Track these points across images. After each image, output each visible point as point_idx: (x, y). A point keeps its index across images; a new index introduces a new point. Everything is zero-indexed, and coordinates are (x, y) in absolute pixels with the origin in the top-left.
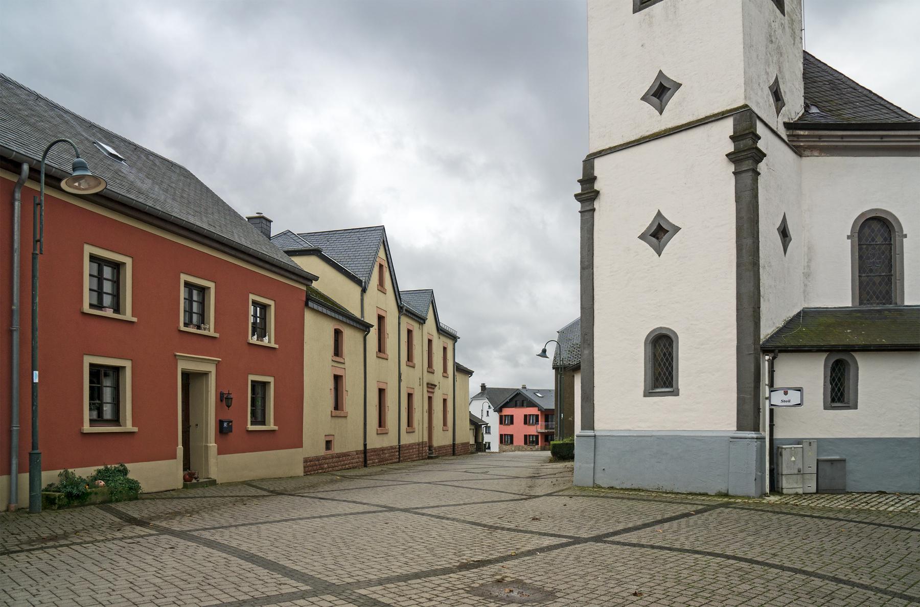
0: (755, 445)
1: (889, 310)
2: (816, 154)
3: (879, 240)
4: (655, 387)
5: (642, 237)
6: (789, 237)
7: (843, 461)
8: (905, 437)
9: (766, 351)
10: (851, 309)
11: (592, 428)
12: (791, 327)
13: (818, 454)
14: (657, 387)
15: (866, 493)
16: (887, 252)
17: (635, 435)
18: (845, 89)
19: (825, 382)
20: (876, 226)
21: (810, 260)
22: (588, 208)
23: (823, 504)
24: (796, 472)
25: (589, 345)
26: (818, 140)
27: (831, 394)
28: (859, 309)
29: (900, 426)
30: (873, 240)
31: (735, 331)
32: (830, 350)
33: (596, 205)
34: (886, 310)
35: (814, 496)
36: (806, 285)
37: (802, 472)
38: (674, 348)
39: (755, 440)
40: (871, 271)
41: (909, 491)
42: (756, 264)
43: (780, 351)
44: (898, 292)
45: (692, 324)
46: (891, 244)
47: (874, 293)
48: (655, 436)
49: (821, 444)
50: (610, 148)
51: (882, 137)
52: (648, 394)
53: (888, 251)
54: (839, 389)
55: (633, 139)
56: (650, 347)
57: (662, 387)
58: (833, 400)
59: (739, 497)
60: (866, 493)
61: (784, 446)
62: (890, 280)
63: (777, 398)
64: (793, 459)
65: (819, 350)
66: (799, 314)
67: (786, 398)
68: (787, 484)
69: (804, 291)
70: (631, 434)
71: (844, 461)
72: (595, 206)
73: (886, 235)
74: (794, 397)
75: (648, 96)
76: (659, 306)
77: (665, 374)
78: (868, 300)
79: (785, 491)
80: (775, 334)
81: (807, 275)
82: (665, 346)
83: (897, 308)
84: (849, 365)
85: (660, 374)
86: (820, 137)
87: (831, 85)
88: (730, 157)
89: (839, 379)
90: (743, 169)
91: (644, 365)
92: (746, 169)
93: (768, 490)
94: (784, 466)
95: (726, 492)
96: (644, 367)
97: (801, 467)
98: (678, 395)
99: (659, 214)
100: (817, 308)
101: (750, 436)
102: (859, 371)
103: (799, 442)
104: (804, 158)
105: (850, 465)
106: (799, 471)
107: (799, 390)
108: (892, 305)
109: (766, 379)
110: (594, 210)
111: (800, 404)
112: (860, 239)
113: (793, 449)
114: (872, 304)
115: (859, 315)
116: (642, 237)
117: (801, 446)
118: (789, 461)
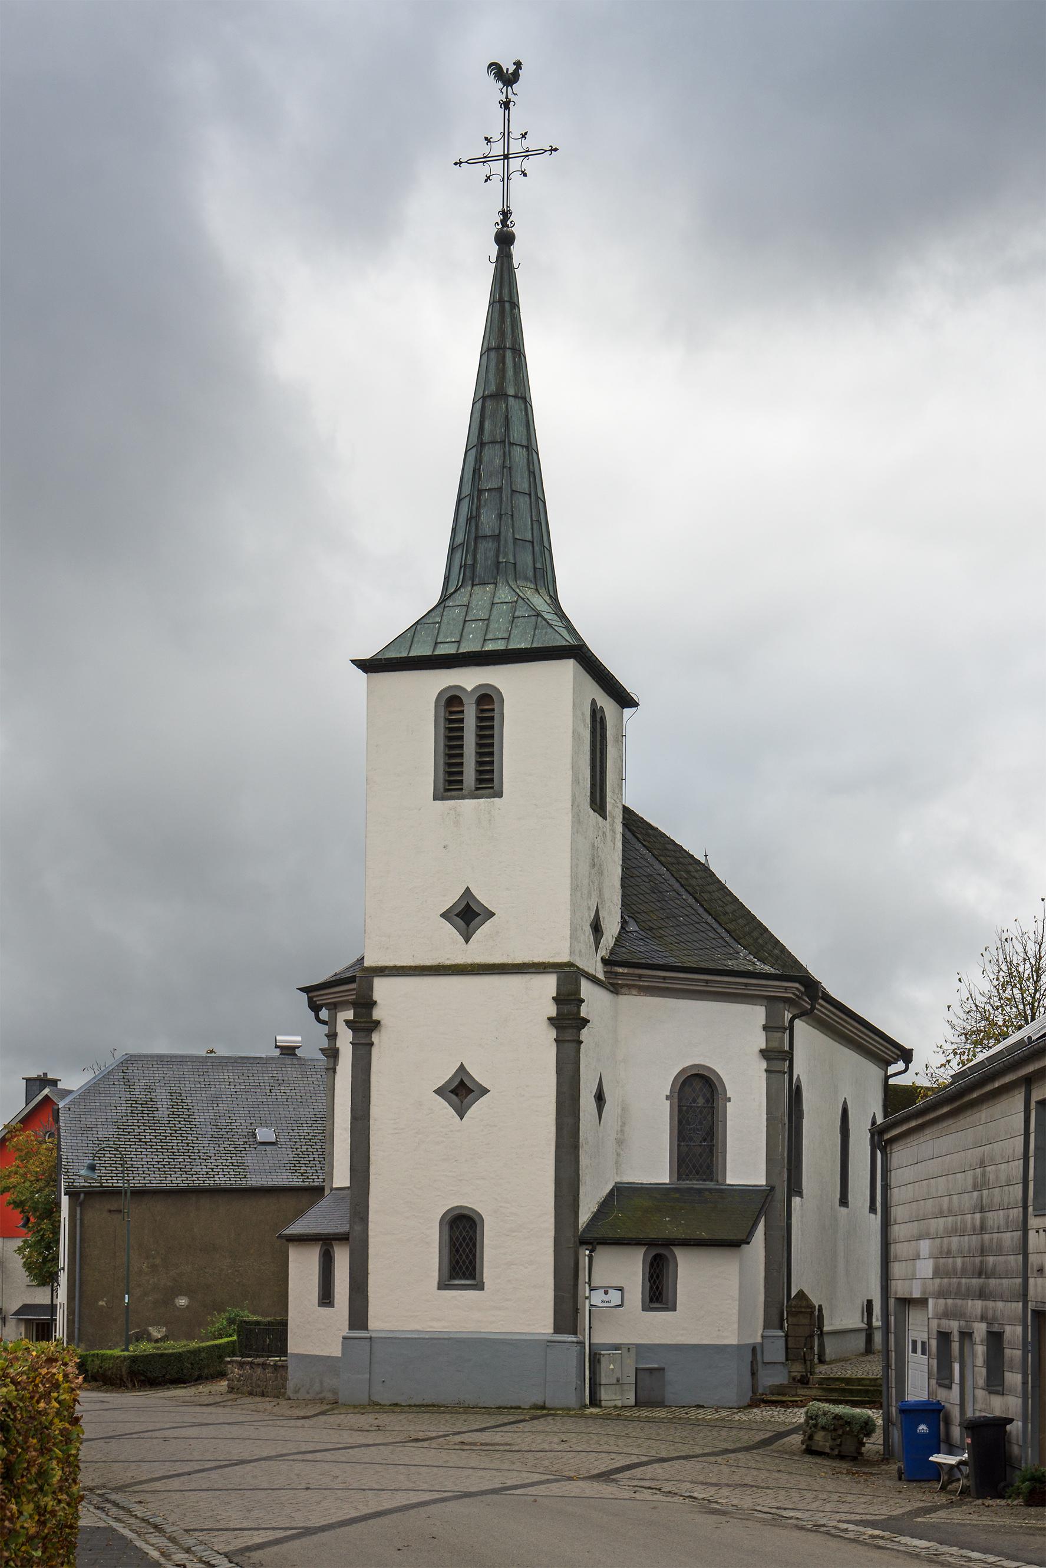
0: (576, 1349)
1: (710, 1190)
2: (634, 992)
3: (701, 1101)
4: (452, 1277)
5: (439, 1092)
6: (603, 1101)
7: (661, 1370)
8: (723, 1343)
9: (583, 1242)
10: (668, 1186)
11: (365, 1327)
12: (605, 1211)
13: (637, 1362)
14: (454, 1278)
15: (684, 1407)
16: (709, 1118)
17: (427, 1337)
18: (668, 892)
19: (643, 1279)
20: (698, 1085)
21: (624, 1124)
22: (363, 1041)
23: (646, 1414)
24: (615, 1381)
25: (362, 1218)
26: (637, 979)
27: (650, 1293)
28: (677, 1186)
29: (719, 1330)
30: (694, 1101)
31: (552, 1220)
32: (649, 1243)
33: (375, 1038)
34: (706, 1189)
35: (634, 1409)
36: (618, 1155)
37: (621, 1382)
38: (478, 1232)
39: (576, 1345)
40: (691, 1139)
41: (727, 1405)
42: (575, 1147)
43: (599, 1244)
44: (719, 1166)
45: (501, 1207)
46: (714, 1107)
47: (694, 1166)
48: (453, 1338)
49: (641, 1349)
50: (395, 968)
51: (707, 981)
52: (442, 1286)
53: (710, 1116)
54: (657, 1288)
55: (428, 963)
56: (446, 1229)
57: (461, 1278)
58: (651, 1300)
59: (558, 1409)
60: (684, 1407)
61: (602, 1352)
62: (711, 1151)
63: (597, 1298)
64: (612, 1367)
65: (636, 1242)
66: (611, 1193)
67: (606, 1298)
68: (606, 1396)
69: (616, 1163)
70: (421, 1336)
71: (663, 1369)
72: (373, 1039)
73: (708, 1095)
74: (615, 1297)
75: (450, 915)
76: (460, 1180)
77: (464, 1262)
78: (687, 1175)
79: (603, 1403)
80: (590, 1221)
81: (620, 1142)
82: (464, 1228)
83: (718, 1187)
84: (669, 1261)
85: (457, 1262)
86: (640, 976)
87: (651, 883)
88: (553, 1022)
89: (658, 1277)
90: (567, 1039)
91: (438, 1250)
92: (569, 1039)
93: (587, 1401)
94: (603, 1374)
95: (542, 1404)
96: (438, 1252)
97: (620, 1376)
98: (482, 1289)
99: (462, 1067)
100: (631, 1183)
101: (570, 1339)
102: (679, 1268)
103: (617, 1347)
104: (621, 996)
105: (670, 1375)
106: (618, 1381)
107: (620, 1289)
108: (713, 1183)
109: (584, 1276)
110: (372, 1044)
111: (620, 1305)
112: (680, 1100)
113: (611, 1355)
114: (691, 1180)
115: (677, 1195)
116: (439, 1092)
117: (620, 1352)
118: (609, 1368)
